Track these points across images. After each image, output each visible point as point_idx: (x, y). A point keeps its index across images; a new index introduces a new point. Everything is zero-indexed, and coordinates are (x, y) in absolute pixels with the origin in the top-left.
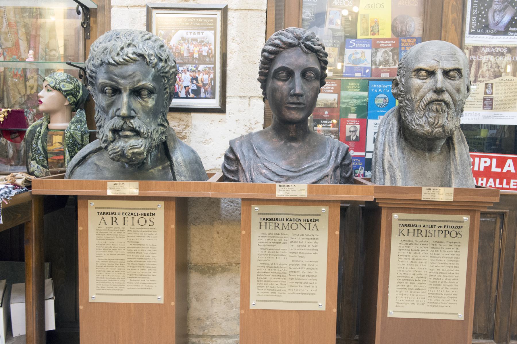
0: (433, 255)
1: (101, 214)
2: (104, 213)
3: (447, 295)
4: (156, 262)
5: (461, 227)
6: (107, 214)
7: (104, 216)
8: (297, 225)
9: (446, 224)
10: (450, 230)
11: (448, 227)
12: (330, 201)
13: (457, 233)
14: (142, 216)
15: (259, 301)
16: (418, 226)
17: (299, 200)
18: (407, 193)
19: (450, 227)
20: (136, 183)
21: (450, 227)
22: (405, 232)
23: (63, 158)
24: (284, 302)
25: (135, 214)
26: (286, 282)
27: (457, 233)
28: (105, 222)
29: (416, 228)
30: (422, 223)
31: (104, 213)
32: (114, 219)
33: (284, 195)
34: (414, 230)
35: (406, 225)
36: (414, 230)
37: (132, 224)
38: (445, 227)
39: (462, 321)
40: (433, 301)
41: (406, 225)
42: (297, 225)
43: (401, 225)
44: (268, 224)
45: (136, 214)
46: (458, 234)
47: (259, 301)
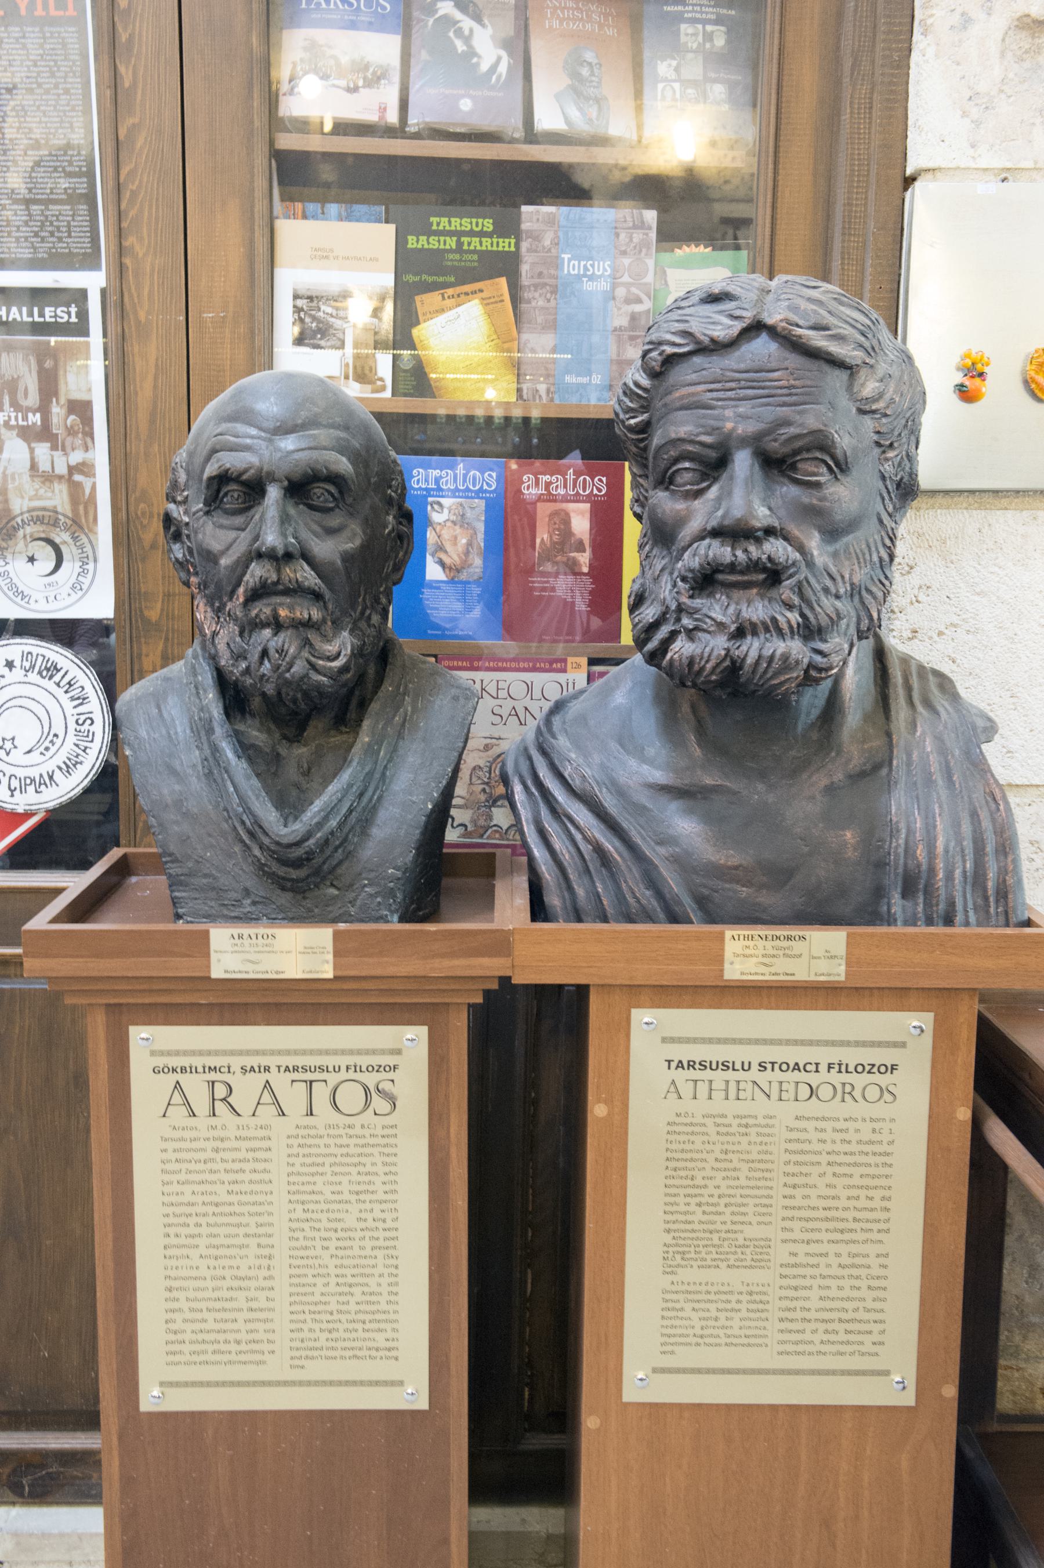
0: (298, 1168)
1: (287, 1069)
2: (183, 1070)
3: (732, 1310)
4: (886, 1278)
5: (894, 1068)
6: (193, 1070)
7: (184, 1079)
8: (834, 1087)
9: (350, 1060)
10: (814, 1079)
11: (842, 1068)
12: (687, 987)
13: (881, 1089)
14: (351, 1075)
15: (171, 1384)
16: (738, 1066)
17: (738, 987)
18: (189, 956)
19: (364, 1069)
20: (323, 936)
21: (851, 1068)
22: (686, 1090)
23: (511, 820)
24: (317, 1383)
25: (808, 1067)
26: (781, 1320)
27: (881, 1089)
28: (276, 1102)
29: (730, 1075)
30: (824, 1056)
31: (183, 1070)
32: (221, 1091)
33: (243, 968)
34: (727, 1082)
35: (691, 1065)
36: (727, 1082)
37: (303, 1109)
38: (830, 1067)
39: (908, 1408)
40: (210, 1325)
41: (691, 1065)
42: (834, 1087)
43: (674, 1065)
44: (733, 1086)
45: (813, 1068)
46: (885, 1093)
47: (171, 1384)
